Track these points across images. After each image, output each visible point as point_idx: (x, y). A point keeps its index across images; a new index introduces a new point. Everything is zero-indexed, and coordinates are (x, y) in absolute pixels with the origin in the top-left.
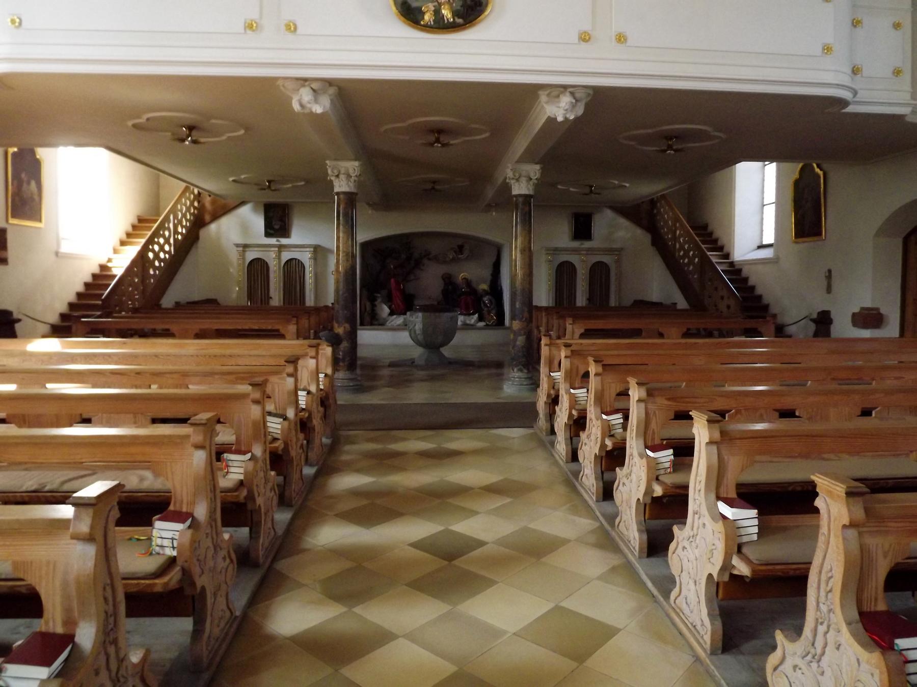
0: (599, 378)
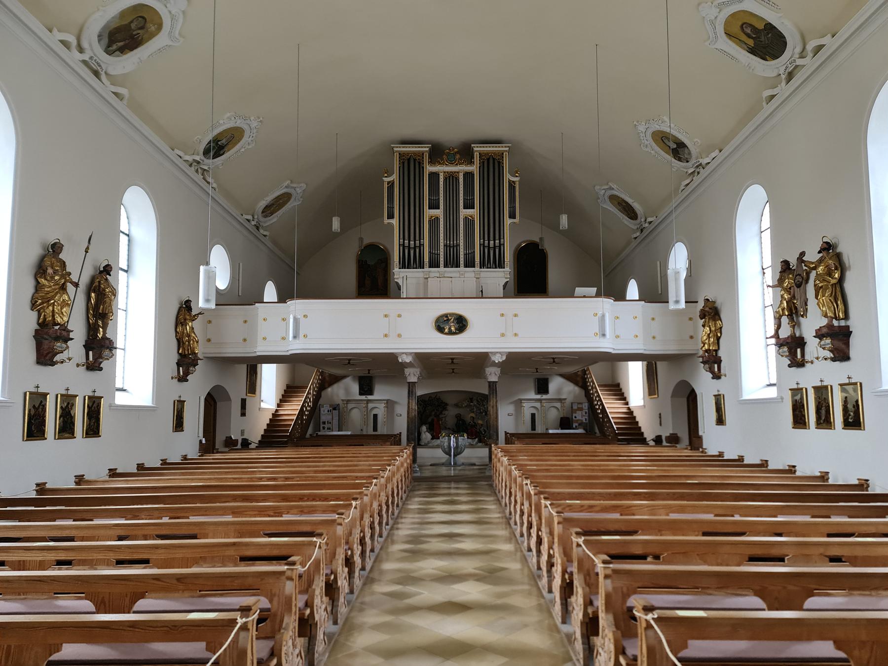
0: (561, 526)
